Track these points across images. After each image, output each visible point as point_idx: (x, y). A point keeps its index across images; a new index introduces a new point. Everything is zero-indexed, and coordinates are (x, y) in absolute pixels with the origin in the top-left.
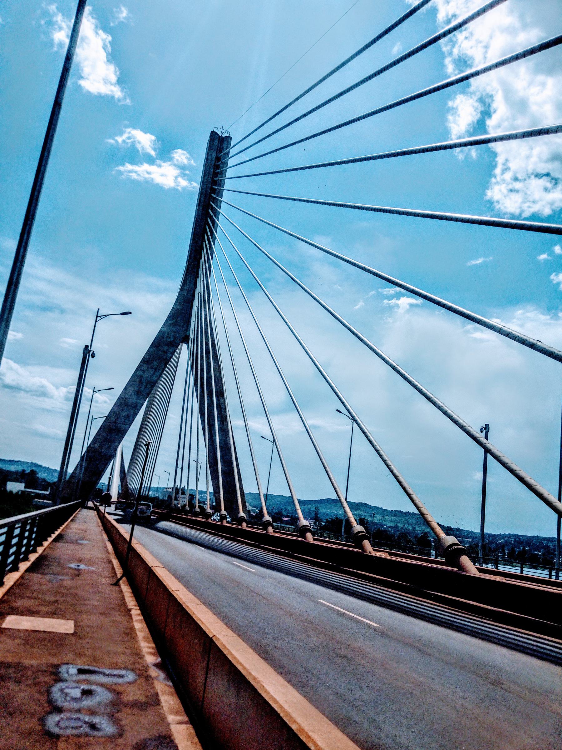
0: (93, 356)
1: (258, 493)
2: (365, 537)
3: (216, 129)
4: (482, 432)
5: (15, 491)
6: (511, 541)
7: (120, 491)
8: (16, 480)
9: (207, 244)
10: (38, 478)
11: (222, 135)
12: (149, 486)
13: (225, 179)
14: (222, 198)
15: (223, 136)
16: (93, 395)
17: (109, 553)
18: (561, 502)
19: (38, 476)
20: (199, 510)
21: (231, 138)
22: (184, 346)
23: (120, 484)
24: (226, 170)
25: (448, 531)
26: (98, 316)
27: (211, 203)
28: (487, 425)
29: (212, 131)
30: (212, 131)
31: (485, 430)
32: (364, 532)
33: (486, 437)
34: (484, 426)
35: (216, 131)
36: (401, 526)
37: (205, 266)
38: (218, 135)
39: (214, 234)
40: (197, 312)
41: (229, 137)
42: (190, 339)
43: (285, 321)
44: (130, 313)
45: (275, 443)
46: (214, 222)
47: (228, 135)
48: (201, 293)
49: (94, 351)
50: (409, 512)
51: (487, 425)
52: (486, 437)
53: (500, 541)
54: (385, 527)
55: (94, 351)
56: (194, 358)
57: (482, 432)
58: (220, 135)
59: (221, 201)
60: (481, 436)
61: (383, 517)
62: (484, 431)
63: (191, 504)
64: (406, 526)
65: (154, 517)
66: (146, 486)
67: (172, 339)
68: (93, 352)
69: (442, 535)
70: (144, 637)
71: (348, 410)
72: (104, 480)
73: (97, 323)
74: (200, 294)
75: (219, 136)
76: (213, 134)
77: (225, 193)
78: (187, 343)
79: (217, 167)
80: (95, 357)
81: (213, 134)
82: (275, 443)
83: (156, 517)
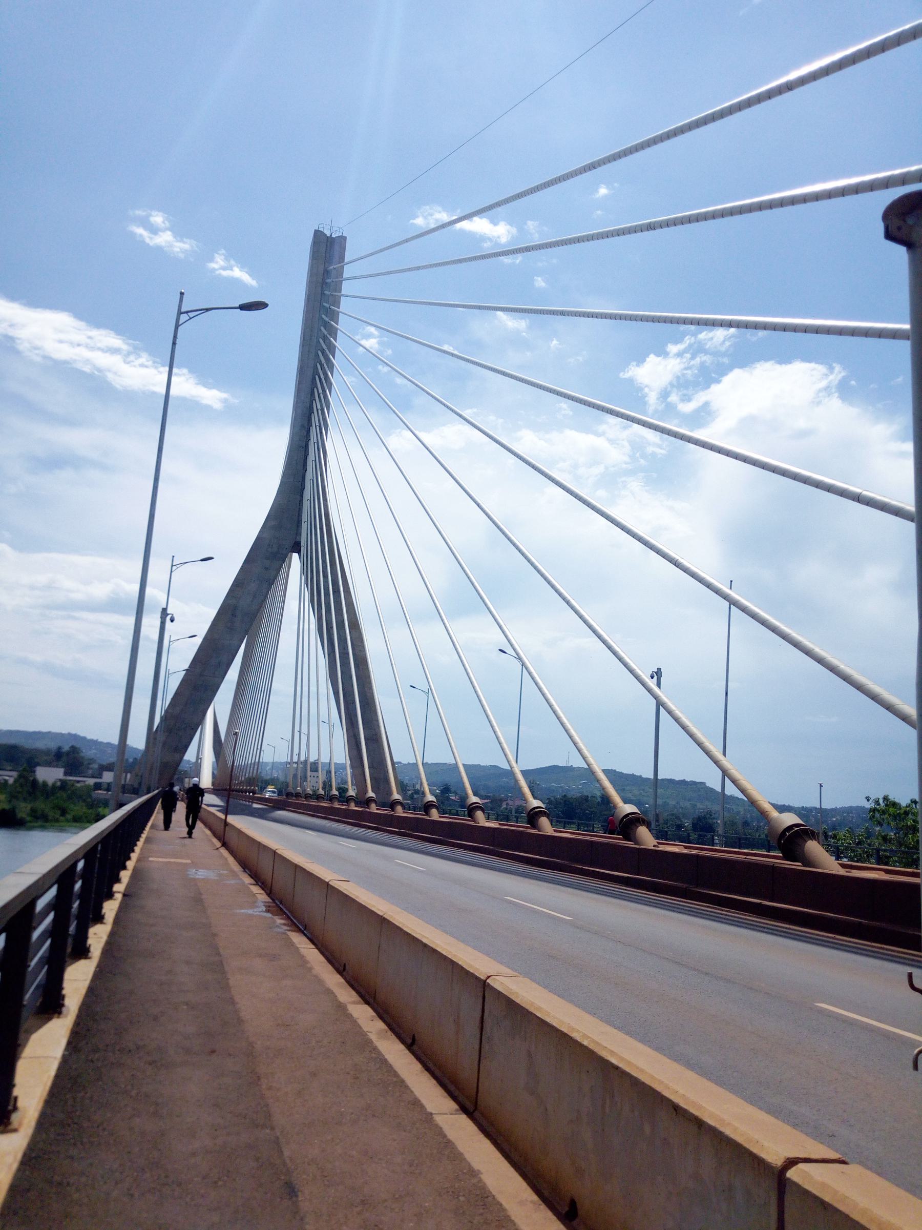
0: (172, 620)
1: (455, 763)
2: (543, 813)
3: (322, 226)
4: (652, 677)
5: (50, 782)
6: (853, 817)
7: (216, 772)
8: (49, 764)
9: (320, 391)
10: (83, 758)
11: (331, 235)
12: (257, 760)
13: (342, 281)
14: (339, 308)
15: (333, 236)
16: (169, 646)
17: (207, 835)
18: (725, 756)
19: (82, 755)
20: (337, 793)
21: (346, 237)
22: (295, 556)
23: (214, 760)
24: (343, 267)
25: (782, 809)
26: (174, 564)
27: (323, 316)
28: (659, 669)
29: (315, 230)
30: (315, 230)
31: (657, 675)
32: (543, 808)
33: (659, 685)
34: (656, 671)
35: (321, 229)
36: (674, 803)
37: (317, 440)
38: (326, 235)
39: (329, 378)
40: (309, 512)
41: (342, 237)
42: (302, 548)
43: (409, 550)
44: (211, 558)
45: (431, 690)
46: (328, 360)
47: (340, 234)
48: (313, 480)
49: (173, 615)
50: (685, 780)
51: (659, 669)
52: (659, 685)
53: (834, 819)
54: (647, 806)
55: (173, 615)
56: (308, 570)
57: (652, 677)
58: (329, 235)
59: (338, 313)
60: (652, 684)
61: (643, 790)
62: (656, 677)
63: (327, 785)
64: (681, 803)
65: (263, 807)
66: (253, 761)
67: (275, 549)
68: (171, 615)
69: (774, 814)
70: (171, 246)
71: (514, 650)
72: (190, 755)
73: (173, 573)
74: (311, 480)
75: (328, 237)
76: (318, 234)
77: (344, 301)
78: (299, 552)
79: (324, 284)
80: (174, 622)
81: (318, 234)
82: (431, 690)
83: (268, 806)
